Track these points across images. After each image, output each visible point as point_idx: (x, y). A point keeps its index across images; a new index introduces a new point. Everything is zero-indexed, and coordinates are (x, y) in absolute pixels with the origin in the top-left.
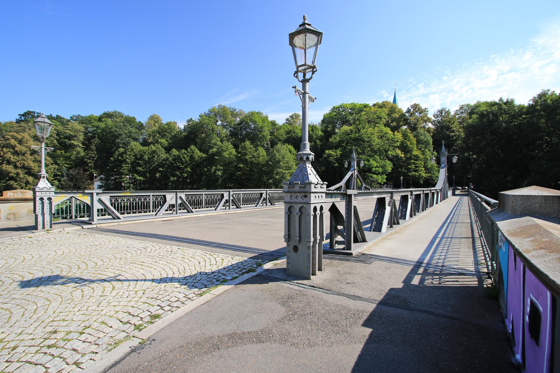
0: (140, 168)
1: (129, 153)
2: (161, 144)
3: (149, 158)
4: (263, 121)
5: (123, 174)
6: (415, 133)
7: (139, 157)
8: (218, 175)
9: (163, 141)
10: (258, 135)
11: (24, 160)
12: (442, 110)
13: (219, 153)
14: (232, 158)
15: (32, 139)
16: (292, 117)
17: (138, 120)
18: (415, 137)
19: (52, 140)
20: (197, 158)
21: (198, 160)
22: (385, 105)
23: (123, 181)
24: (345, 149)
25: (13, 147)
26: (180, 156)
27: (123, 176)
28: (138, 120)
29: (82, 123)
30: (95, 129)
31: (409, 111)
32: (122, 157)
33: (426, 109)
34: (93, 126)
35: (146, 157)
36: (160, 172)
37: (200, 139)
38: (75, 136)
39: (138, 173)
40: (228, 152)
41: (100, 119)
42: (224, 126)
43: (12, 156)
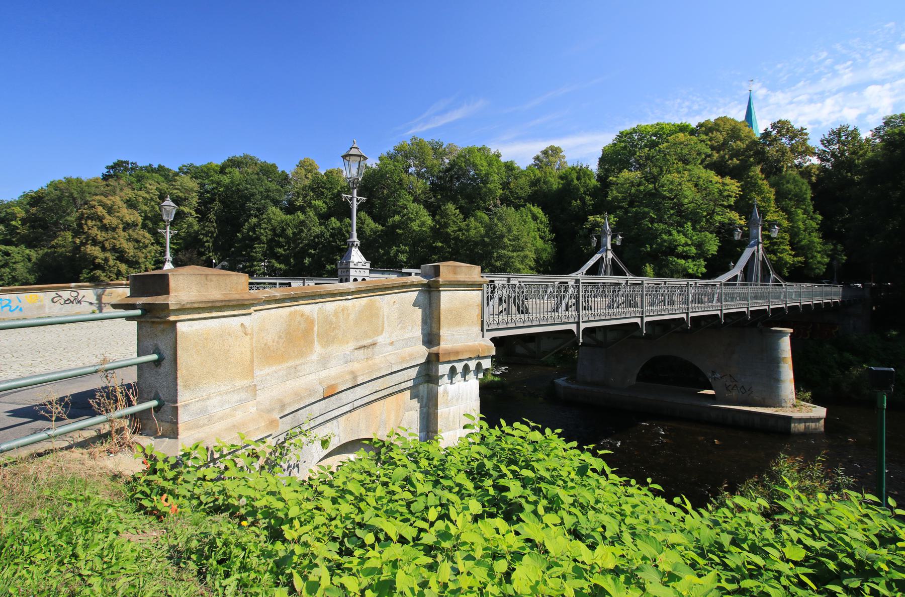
0: (281, 250)
1: (264, 226)
2: (316, 208)
3: (294, 233)
4: (490, 164)
5: (254, 259)
6: (773, 178)
7: (278, 231)
8: (401, 261)
9: (318, 203)
10: (480, 188)
11: (114, 238)
12: (839, 131)
13: (403, 223)
14: (425, 232)
15: (125, 206)
16: (545, 153)
17: (280, 170)
18: (772, 186)
19: (153, 207)
20: (368, 232)
21: (370, 236)
22: (718, 125)
23: (255, 271)
24: (626, 211)
25: (100, 219)
26: (341, 230)
27: (255, 263)
28: (280, 170)
29: (196, 178)
30: (215, 185)
31: (766, 134)
32: (254, 232)
33: (802, 129)
34: (213, 182)
35: (290, 232)
36: (310, 255)
37: (379, 199)
38: (185, 199)
39: (278, 258)
40: (418, 222)
41: (222, 170)
42: (420, 175)
43: (99, 233)
